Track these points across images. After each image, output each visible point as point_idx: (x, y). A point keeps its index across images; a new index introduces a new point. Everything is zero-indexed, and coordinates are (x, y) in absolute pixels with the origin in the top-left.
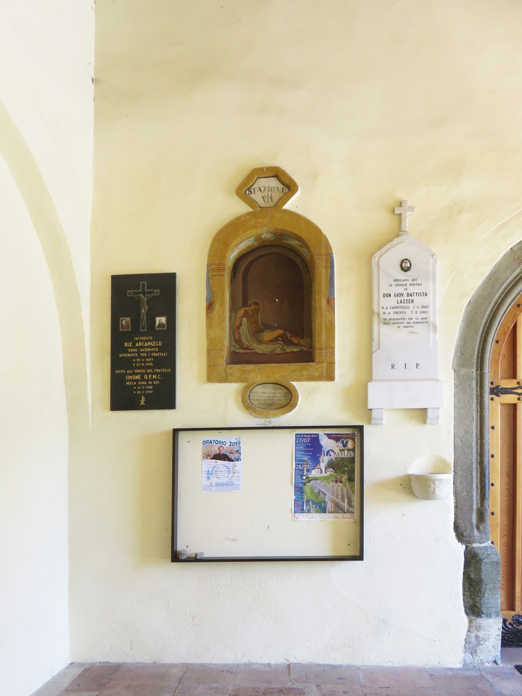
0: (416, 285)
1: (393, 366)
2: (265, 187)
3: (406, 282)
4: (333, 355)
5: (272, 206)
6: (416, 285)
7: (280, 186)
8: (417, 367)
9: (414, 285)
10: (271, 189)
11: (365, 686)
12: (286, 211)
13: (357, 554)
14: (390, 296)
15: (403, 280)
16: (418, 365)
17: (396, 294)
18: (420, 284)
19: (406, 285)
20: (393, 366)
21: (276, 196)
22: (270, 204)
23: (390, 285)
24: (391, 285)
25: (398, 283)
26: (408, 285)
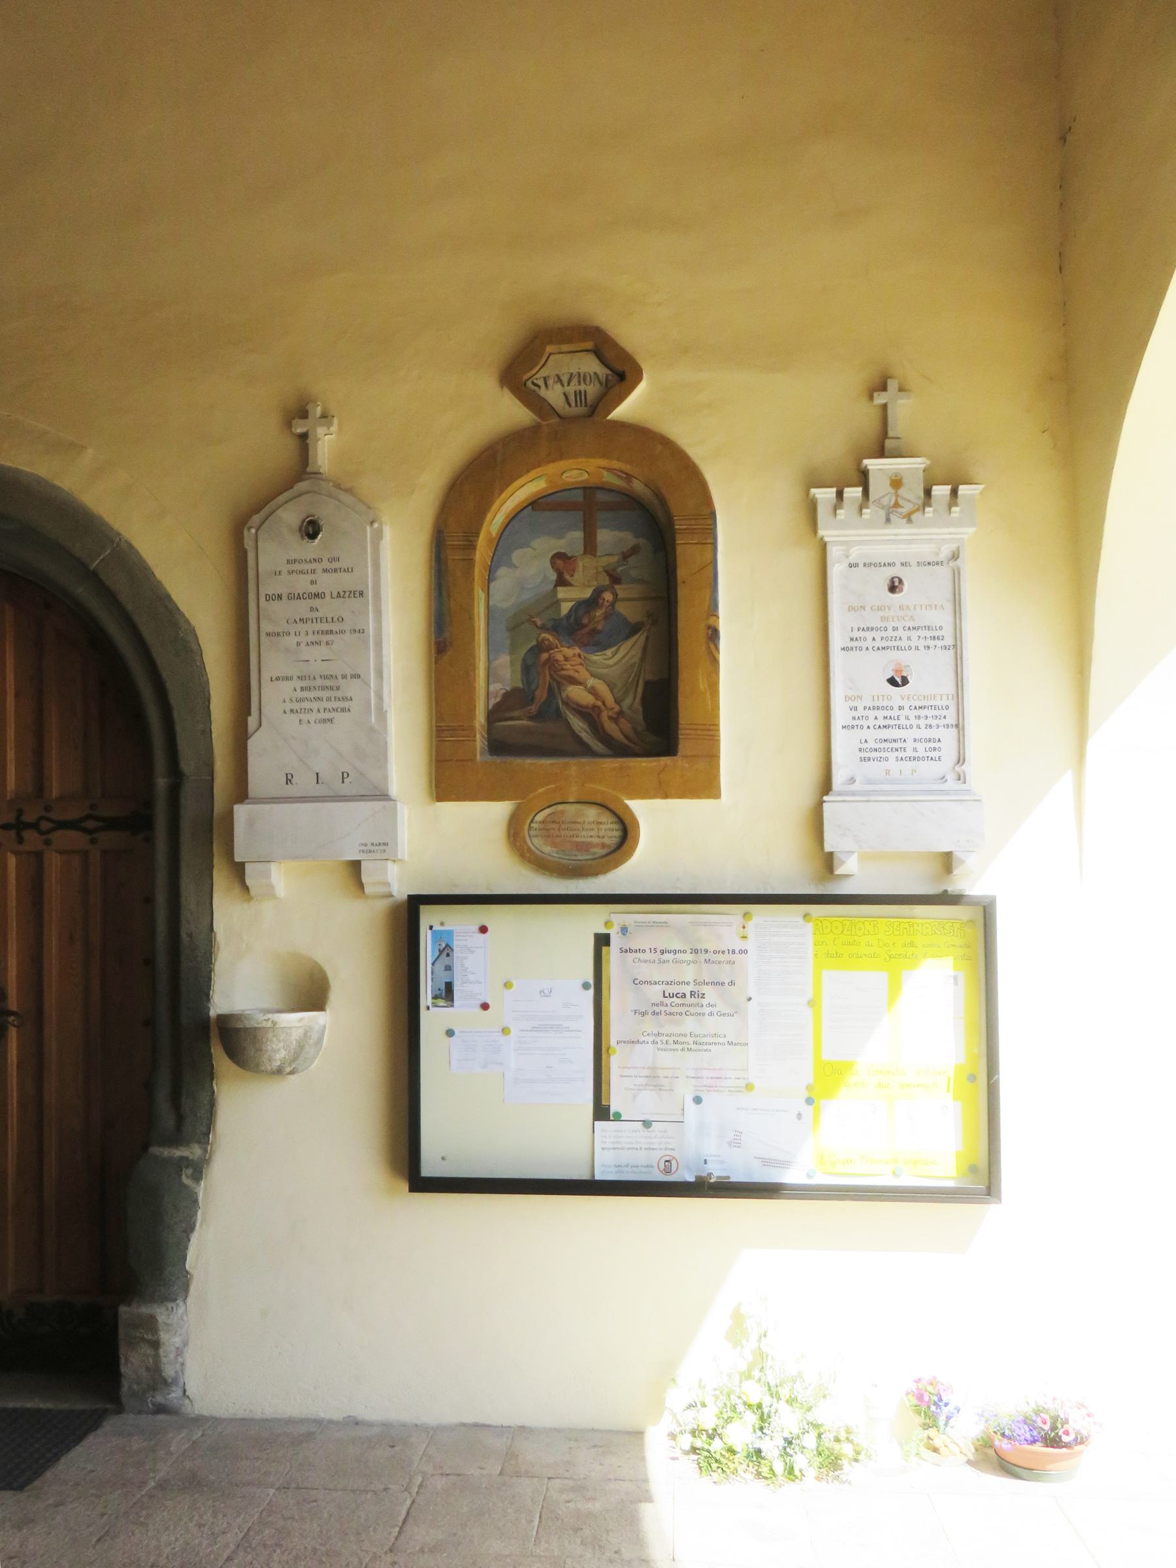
0: (339, 571)
1: (290, 777)
2: (572, 374)
3: (314, 566)
4: (473, 730)
5: (559, 412)
6: (339, 571)
7: (602, 371)
8: (345, 780)
9: (336, 571)
10: (582, 378)
11: (266, 1488)
12: (621, 426)
13: (430, 1167)
14: (281, 599)
15: (882, 564)
16: (345, 775)
17: (305, 593)
18: (350, 570)
19: (313, 571)
20: (290, 777)
21: (592, 390)
22: (581, 410)
23: (277, 573)
24: (280, 572)
25: (297, 567)
26: (319, 571)
